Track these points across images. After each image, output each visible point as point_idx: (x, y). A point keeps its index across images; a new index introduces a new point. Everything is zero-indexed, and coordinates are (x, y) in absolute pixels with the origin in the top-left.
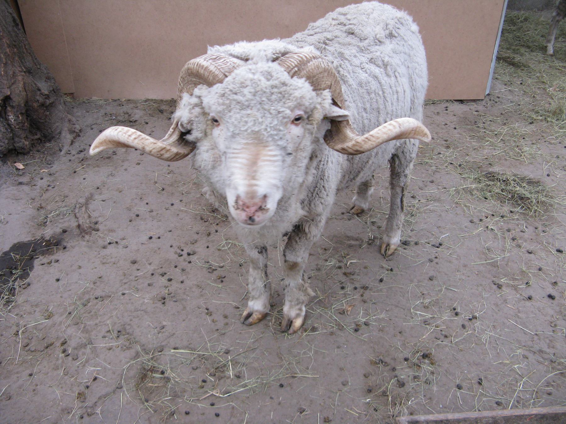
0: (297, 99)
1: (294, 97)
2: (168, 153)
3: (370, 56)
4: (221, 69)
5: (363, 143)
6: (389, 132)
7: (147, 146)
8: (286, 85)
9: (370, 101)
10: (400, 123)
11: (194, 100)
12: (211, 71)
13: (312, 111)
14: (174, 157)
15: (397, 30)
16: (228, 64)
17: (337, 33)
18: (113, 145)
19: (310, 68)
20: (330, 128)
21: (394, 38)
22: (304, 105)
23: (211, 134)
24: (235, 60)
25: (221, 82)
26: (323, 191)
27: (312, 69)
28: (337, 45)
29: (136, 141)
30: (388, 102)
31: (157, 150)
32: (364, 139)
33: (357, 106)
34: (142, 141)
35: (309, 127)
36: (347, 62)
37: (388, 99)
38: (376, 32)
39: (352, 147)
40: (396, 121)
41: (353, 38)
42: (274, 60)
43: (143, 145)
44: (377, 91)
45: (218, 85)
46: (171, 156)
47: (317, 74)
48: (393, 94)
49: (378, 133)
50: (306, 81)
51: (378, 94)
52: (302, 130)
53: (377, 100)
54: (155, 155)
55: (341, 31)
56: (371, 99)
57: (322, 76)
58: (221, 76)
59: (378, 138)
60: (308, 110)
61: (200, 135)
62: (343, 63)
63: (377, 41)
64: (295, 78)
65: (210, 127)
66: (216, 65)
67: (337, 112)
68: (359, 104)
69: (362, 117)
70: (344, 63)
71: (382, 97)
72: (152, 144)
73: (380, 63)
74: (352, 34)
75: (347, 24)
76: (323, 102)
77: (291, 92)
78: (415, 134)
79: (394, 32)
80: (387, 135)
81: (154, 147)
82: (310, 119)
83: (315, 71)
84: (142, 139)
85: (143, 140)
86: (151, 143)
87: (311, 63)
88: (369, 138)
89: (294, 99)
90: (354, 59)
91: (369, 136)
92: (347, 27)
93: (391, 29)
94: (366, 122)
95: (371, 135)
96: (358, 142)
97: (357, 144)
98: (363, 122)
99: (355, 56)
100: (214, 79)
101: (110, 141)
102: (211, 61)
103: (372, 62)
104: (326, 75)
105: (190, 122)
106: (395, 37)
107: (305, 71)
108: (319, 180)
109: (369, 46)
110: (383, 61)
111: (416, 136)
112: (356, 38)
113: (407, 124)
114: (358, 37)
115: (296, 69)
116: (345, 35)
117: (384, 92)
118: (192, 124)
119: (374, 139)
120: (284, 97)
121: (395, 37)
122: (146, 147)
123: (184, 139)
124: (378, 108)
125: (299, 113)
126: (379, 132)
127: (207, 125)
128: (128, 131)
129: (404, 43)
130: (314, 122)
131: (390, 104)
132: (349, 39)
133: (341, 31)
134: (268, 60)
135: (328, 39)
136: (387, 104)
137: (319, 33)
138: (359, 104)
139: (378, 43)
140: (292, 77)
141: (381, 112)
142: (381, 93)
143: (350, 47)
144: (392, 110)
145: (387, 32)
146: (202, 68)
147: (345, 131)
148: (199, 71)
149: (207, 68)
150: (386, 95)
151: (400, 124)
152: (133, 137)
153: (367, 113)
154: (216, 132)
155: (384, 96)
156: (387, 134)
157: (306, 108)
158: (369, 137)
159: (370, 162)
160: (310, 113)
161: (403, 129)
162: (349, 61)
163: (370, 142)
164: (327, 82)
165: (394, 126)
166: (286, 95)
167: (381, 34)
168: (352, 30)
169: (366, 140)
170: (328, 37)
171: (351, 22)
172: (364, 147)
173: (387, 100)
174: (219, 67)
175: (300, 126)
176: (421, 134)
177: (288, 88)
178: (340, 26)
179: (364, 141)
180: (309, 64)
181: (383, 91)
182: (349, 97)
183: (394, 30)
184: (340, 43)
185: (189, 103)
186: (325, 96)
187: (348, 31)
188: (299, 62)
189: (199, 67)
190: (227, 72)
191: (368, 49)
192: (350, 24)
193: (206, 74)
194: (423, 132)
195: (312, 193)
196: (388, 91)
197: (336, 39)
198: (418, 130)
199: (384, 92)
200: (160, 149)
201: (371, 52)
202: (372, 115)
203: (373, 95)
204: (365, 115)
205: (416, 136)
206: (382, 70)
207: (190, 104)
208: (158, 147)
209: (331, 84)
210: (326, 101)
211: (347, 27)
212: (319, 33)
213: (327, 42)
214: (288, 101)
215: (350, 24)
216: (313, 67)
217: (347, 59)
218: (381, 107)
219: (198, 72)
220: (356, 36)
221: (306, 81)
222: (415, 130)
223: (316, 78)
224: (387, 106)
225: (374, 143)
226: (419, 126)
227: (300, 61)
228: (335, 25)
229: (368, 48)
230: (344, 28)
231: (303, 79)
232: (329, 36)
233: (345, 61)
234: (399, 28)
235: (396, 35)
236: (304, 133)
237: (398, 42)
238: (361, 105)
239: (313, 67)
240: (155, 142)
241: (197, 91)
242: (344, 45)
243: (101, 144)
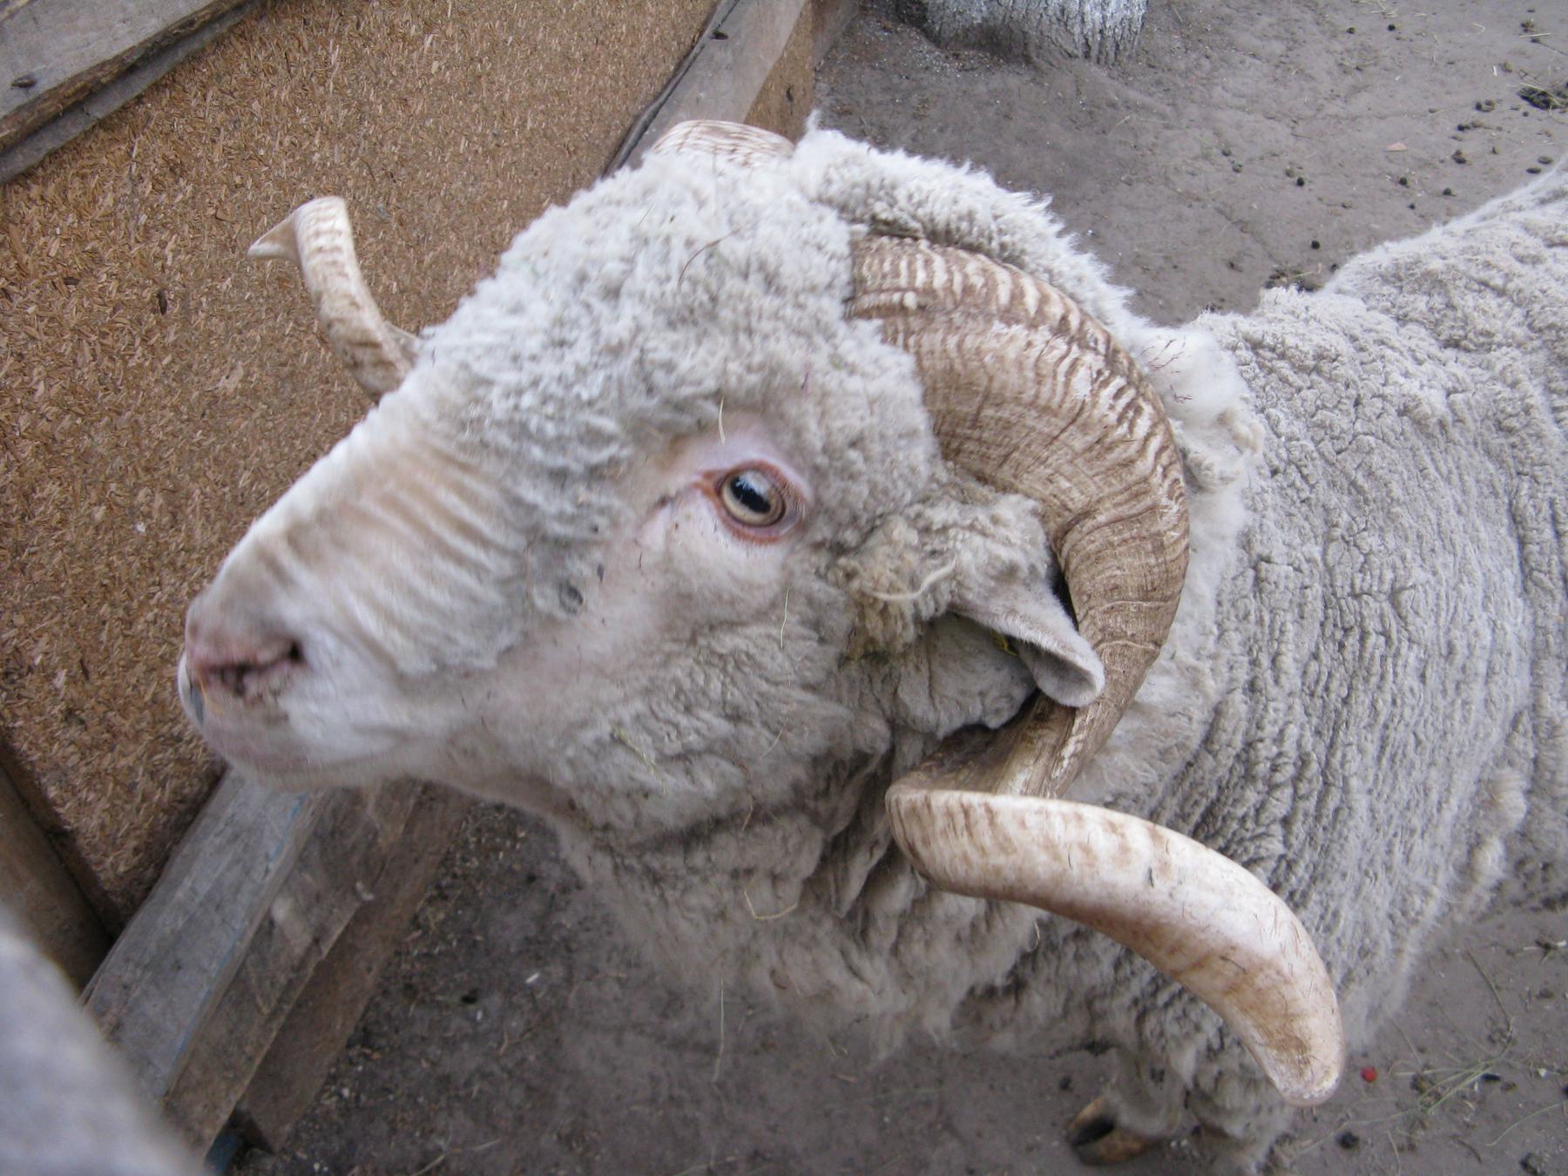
6: (1077, 856)
10: (1174, 859)
19: (994, 344)
27: (1000, 359)
32: (956, 809)
40: (746, 637)
47: (1017, 400)
49: (1023, 824)
59: (1005, 845)
72: (346, 302)
78: (1233, 989)
80: (1056, 867)
81: (345, 315)
84: (334, 263)
85: (333, 270)
86: (347, 296)
91: (981, 811)
95: (989, 810)
96: (929, 806)
107: (952, 341)
113: (1213, 900)
115: (910, 300)
119: (987, 841)
122: (325, 298)
126: (1032, 820)
147: (1015, 766)
151: (1165, 866)
156: (1056, 857)
158: (980, 812)
161: (1158, 896)
163: (965, 839)
165: (1124, 849)
176: (1274, 1025)
180: (998, 326)
188: (957, 287)
198: (1260, 981)
200: (358, 337)
208: (355, 324)
209: (1087, 514)
225: (975, 857)
226: (1284, 966)
240: (358, 300)
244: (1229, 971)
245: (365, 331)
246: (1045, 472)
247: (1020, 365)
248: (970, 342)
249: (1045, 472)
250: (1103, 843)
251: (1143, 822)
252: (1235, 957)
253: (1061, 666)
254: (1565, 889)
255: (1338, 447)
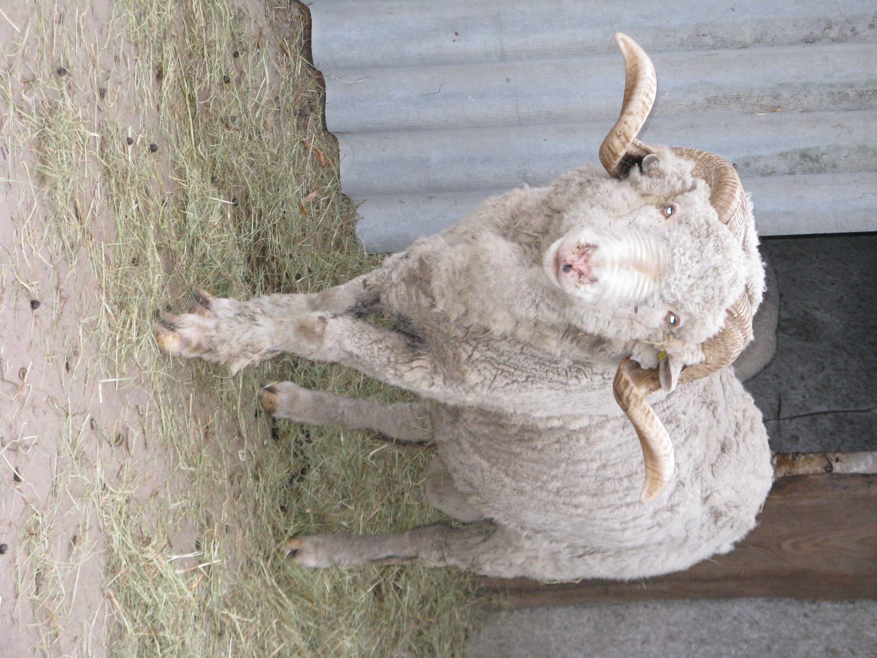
0: (703, 319)
1: (705, 315)
2: (620, 145)
3: (687, 482)
4: (733, 217)
5: (642, 407)
7: (634, 119)
8: (720, 304)
9: (617, 477)
11: (690, 181)
12: (730, 203)
13: (680, 338)
14: (612, 152)
15: (729, 525)
16: (739, 226)
17: (724, 425)
18: (631, 69)
20: (643, 367)
21: (714, 519)
22: (692, 328)
23: (647, 204)
24: (742, 236)
25: (720, 219)
26: (506, 381)
27: (733, 336)
28: (707, 424)
29: (641, 105)
30: (610, 512)
31: (627, 132)
33: (612, 450)
34: (641, 113)
35: (661, 335)
36: (683, 438)
37: (616, 512)
38: (723, 492)
39: (634, 394)
41: (715, 451)
42: (747, 289)
43: (635, 113)
44: (632, 492)
45: (716, 217)
46: (616, 149)
48: (622, 523)
50: (721, 328)
51: (627, 495)
52: (657, 325)
53: (617, 491)
54: (619, 129)
55: (728, 431)
56: (621, 479)
57: (722, 349)
58: (726, 217)
60: (682, 333)
61: (644, 188)
62: (681, 432)
63: (708, 493)
64: (726, 314)
65: (655, 201)
66: (738, 210)
67: (676, 372)
68: (614, 455)
69: (592, 460)
70: (682, 435)
71: (620, 502)
72: (635, 126)
73: (675, 500)
74: (723, 450)
75: (738, 438)
76: (690, 352)
77: (713, 311)
78: (653, 478)
79: (724, 519)
82: (671, 337)
83: (730, 341)
86: (638, 124)
87: (741, 334)
88: (649, 415)
89: (702, 315)
90: (685, 453)
92: (733, 439)
93: (730, 515)
94: (584, 466)
97: (640, 400)
98: (585, 460)
99: (690, 455)
100: (721, 208)
101: (636, 65)
102: (741, 202)
103: (678, 485)
104: (722, 356)
105: (661, 175)
106: (716, 522)
107: (732, 327)
108: (525, 374)
109: (702, 479)
110: (678, 504)
111: (649, 480)
112: (715, 457)
114: (717, 461)
115: (736, 315)
116: (721, 437)
117: (628, 505)
118: (659, 177)
120: (707, 302)
121: (716, 522)
123: (633, 164)
124: (603, 495)
125: (681, 322)
126: (659, 427)
127: (658, 197)
128: (652, 91)
129: (705, 537)
130: (666, 341)
131: (606, 516)
132: (716, 446)
133: (728, 431)
134: (747, 279)
135: (716, 408)
136: (608, 510)
137: (724, 391)
138: (614, 455)
139: (704, 495)
140: (728, 311)
141: (596, 499)
142: (629, 499)
143: (703, 446)
144: (595, 519)
145: (723, 509)
146: (732, 191)
148: (727, 187)
149: (733, 197)
150: (624, 509)
152: (647, 101)
153: (598, 470)
154: (654, 212)
155: (622, 505)
156: (656, 437)
157: (688, 331)
158: (650, 415)
159: (507, 480)
160: (678, 336)
162: (683, 444)
164: (711, 358)
165: (667, 447)
166: (709, 305)
167: (717, 501)
168: (729, 450)
169: (646, 412)
170: (719, 409)
171: (741, 445)
172: (636, 409)
173: (614, 511)
174: (735, 214)
175: (663, 322)
177: (717, 307)
178: (734, 427)
179: (645, 408)
180: (739, 331)
181: (632, 503)
182: (629, 435)
183: (727, 519)
184: (710, 428)
185: (685, 172)
186: (697, 355)
187: (727, 442)
189: (733, 187)
190: (731, 224)
191: (697, 478)
192: (738, 444)
193: (726, 197)
194: (655, 490)
195: (504, 364)
196: (630, 513)
197: (715, 421)
198: (658, 482)
199: (628, 505)
200: (628, 135)
201: (692, 483)
202: (593, 479)
203: (626, 483)
204: (594, 466)
205: (649, 480)
206: (665, 502)
207: (683, 173)
210: (691, 356)
211: (733, 439)
212: (724, 391)
213: (711, 408)
214: (701, 308)
215: (738, 444)
216: (735, 338)
217: (686, 439)
218: (604, 500)
219: (726, 185)
220: (719, 457)
221: (721, 328)
222: (658, 479)
223: (721, 342)
224: (604, 511)
227: (744, 320)
228: (736, 417)
229: (699, 478)
230: (731, 435)
231: (724, 326)
232: (720, 410)
233: (684, 436)
234: (732, 527)
235: (720, 524)
236: (651, 329)
237: (706, 528)
238: (612, 458)
239: (735, 338)
241: (702, 184)
242: (707, 435)
243: (631, 52)
244: (656, 476)
245: (631, 136)
246: (712, 353)
247: (734, 340)
248: (733, 330)
249: (712, 353)
250: (665, 443)
251: (584, 327)
252: (660, 477)
253: (668, 378)
254: (263, 2)
255: (715, 288)
